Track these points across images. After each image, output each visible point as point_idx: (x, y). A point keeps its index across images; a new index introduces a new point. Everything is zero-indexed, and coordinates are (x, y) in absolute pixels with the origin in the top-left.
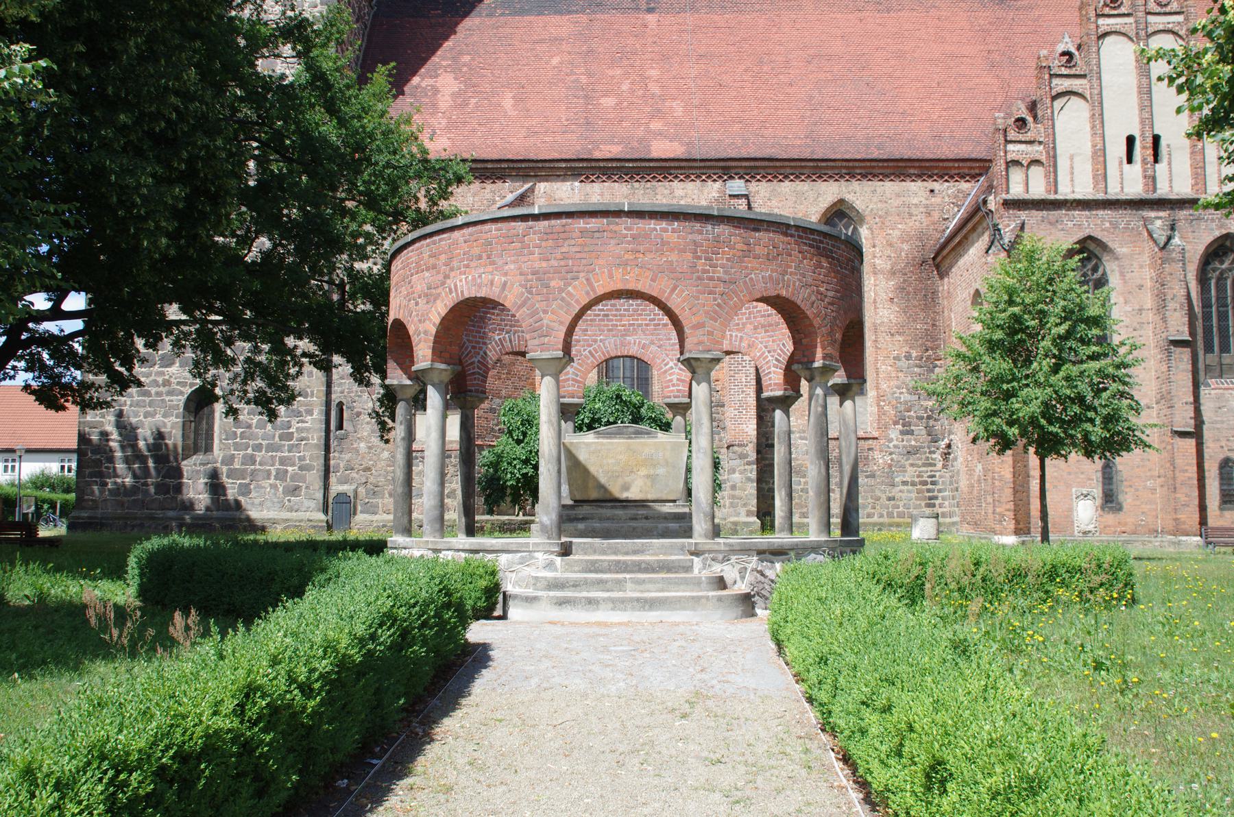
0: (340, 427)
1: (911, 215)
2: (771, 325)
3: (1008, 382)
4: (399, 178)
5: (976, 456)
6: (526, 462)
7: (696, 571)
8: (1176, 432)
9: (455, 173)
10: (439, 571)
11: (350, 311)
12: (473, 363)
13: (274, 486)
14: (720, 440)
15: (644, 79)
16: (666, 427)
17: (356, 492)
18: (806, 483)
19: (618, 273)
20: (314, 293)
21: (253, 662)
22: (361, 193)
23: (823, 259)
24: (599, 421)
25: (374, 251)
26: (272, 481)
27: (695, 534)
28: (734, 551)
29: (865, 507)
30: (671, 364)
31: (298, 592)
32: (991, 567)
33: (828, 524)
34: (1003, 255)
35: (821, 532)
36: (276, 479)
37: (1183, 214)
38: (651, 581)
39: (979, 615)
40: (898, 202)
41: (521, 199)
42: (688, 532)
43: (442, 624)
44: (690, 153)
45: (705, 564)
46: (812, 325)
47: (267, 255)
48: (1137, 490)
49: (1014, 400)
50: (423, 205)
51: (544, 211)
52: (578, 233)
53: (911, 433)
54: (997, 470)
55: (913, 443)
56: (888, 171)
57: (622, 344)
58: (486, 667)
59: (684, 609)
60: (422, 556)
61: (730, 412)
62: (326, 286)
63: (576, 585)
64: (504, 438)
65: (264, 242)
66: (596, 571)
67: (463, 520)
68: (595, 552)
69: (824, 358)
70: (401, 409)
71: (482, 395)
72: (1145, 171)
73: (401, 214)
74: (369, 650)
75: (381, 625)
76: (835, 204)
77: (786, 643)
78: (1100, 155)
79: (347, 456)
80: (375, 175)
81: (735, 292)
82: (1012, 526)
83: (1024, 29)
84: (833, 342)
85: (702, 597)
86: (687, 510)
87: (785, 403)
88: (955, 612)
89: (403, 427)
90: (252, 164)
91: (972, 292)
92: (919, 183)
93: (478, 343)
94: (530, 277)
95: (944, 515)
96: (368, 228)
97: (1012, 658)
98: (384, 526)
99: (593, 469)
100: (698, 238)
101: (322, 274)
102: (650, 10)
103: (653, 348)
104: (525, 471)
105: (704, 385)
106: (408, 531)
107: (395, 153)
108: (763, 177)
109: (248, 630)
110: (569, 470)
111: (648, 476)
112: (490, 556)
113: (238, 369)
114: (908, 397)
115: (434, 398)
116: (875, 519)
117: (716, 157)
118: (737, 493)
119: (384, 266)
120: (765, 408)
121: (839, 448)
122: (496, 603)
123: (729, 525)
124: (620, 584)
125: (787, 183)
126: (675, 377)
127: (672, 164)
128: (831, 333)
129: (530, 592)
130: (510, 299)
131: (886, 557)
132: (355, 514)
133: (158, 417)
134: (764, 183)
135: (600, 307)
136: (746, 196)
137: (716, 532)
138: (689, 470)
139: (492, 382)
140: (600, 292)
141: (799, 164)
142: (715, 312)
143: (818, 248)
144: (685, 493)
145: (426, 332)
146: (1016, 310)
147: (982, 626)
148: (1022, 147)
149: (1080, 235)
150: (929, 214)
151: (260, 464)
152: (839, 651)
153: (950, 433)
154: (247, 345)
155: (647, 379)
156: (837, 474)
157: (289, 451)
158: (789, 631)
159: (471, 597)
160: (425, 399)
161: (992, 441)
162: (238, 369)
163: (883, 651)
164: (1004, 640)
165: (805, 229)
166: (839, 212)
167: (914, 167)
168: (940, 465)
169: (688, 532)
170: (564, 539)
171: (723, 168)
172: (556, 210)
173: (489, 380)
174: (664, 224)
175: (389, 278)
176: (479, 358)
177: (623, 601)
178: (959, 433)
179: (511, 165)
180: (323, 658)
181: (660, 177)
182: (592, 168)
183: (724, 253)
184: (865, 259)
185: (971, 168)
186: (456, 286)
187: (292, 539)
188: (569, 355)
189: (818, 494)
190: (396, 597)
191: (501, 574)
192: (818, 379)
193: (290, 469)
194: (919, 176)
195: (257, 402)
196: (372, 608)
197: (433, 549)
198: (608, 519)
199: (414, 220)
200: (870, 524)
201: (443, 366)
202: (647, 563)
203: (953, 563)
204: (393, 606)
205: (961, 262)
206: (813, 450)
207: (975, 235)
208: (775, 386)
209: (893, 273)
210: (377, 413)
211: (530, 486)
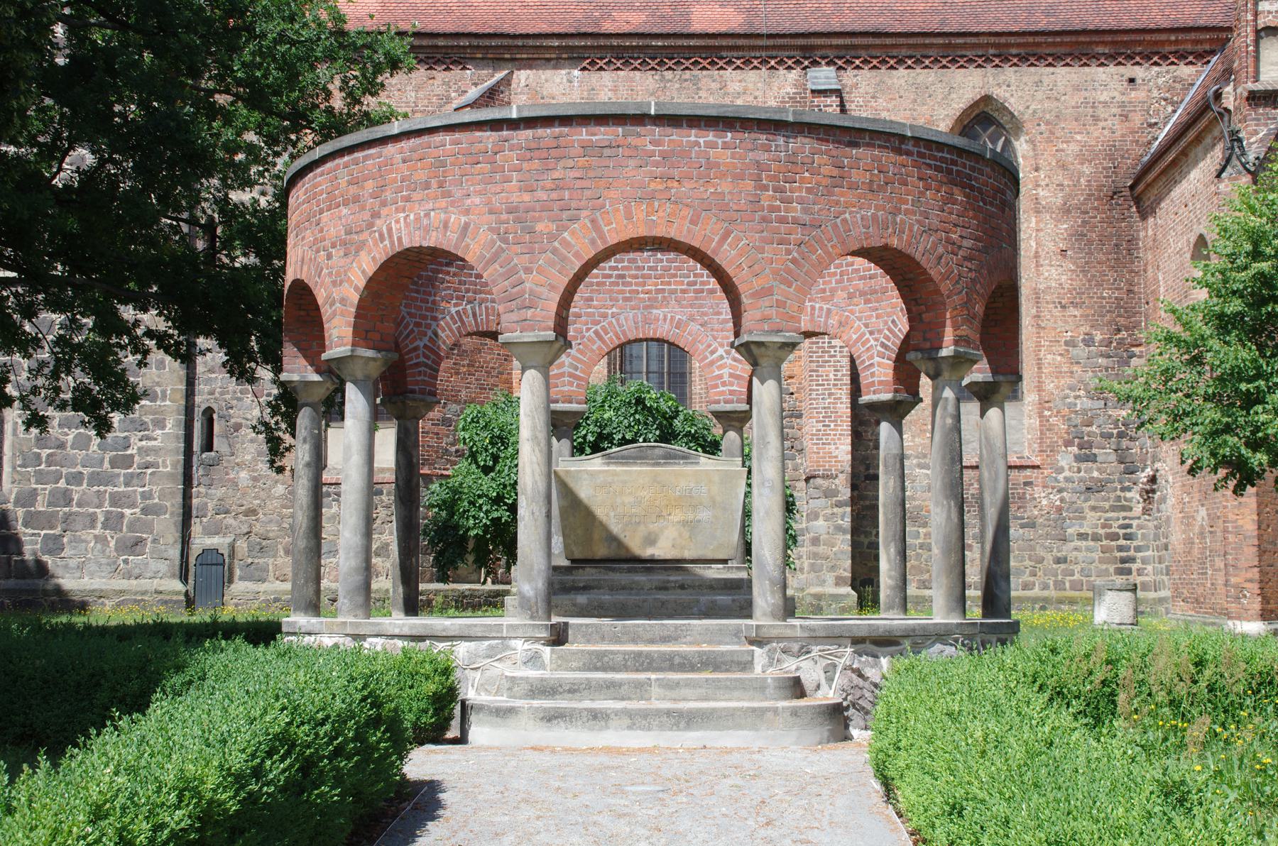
0: (208, 446)
1: (1096, 119)
2: (874, 292)
3: (1249, 381)
4: (300, 59)
5: (1197, 496)
6: (498, 500)
7: (758, 669)
9: (387, 54)
10: (362, 668)
11: (223, 266)
12: (416, 349)
13: (100, 539)
14: (795, 469)
16: (712, 448)
17: (232, 547)
18: (928, 535)
19: (640, 212)
20: (167, 238)
21: (62, 817)
22: (239, 82)
23: (956, 190)
24: (609, 438)
25: (261, 174)
26: (98, 531)
27: (757, 612)
28: (815, 639)
29: (1020, 573)
30: (721, 351)
31: (139, 704)
32: (1222, 669)
33: (963, 599)
34: (1246, 179)
35: (950, 611)
36: (105, 527)
38: (689, 684)
39: (1205, 745)
40: (1078, 98)
41: (491, 96)
42: (745, 610)
43: (366, 750)
44: (751, 24)
45: (771, 659)
46: (937, 292)
47: (88, 177)
49: (1259, 408)
50: (338, 102)
51: (526, 114)
52: (577, 150)
53: (1093, 458)
54: (1231, 517)
55: (1096, 474)
56: (1061, 50)
57: (647, 321)
58: (433, 819)
59: (739, 727)
60: (336, 646)
61: (810, 426)
62: (185, 228)
63: (573, 690)
64: (464, 464)
65: (83, 156)
66: (604, 669)
67: (401, 590)
68: (603, 639)
69: (956, 343)
70: (304, 418)
71: (430, 397)
73: (304, 117)
74: (250, 794)
75: (270, 754)
76: (976, 104)
77: (897, 783)
79: (218, 492)
80: (261, 54)
81: (819, 241)
82: (1256, 605)
84: (971, 317)
85: (767, 709)
86: (743, 575)
87: (896, 411)
88: (1165, 739)
89: (307, 447)
90: (59, 29)
91: (1193, 239)
92: (1112, 69)
93: (425, 317)
94: (504, 216)
95: (1145, 587)
96: (251, 137)
97: (1262, 815)
98: (276, 600)
99: (600, 512)
100: (763, 157)
101: (178, 209)
103: (694, 327)
104: (495, 515)
105: (771, 384)
106: (314, 607)
107: (292, 19)
108: (865, 62)
109: (55, 765)
110: (564, 513)
111: (685, 523)
112: (441, 646)
113: (45, 355)
114: (1088, 403)
115: (355, 401)
116: (1036, 592)
117: (793, 31)
118: (821, 549)
119: (277, 197)
120: (864, 420)
121: (980, 481)
122: (450, 718)
123: (809, 599)
124: (641, 689)
125: (902, 71)
126: (726, 372)
127: (724, 42)
128: (967, 304)
129: (503, 700)
130: (473, 251)
131: (1054, 651)
132: (231, 581)
134: (866, 72)
135: (612, 264)
136: (838, 93)
137: (789, 608)
138: (747, 514)
139: (445, 378)
140: (612, 240)
141: (920, 41)
142: (789, 271)
143: (949, 172)
144: (741, 549)
145: (343, 301)
146: (1265, 266)
147: (1210, 762)
150: (1125, 117)
151: (79, 505)
152: (981, 795)
153: (1155, 459)
154: (58, 318)
155: (683, 375)
156: (976, 521)
157: (127, 485)
158: (902, 764)
159: (412, 707)
160: (343, 403)
161: (1222, 472)
162: (45, 355)
163: (1051, 796)
164: (1247, 785)
165: (929, 143)
166: (984, 116)
167: (1104, 43)
168: (1138, 509)
169: (745, 610)
170: (555, 619)
171: (803, 48)
172: (545, 113)
173: (442, 375)
174: (711, 136)
175: (286, 216)
176: (426, 340)
177: (645, 714)
178: (1167, 463)
179: (475, 42)
180: (178, 807)
181: (705, 63)
182: (600, 47)
183: (803, 180)
184: (1023, 190)
185: (1197, 42)
186: (390, 230)
187: (130, 621)
188: (565, 337)
189: (947, 552)
190: (295, 709)
191: (458, 674)
192: (946, 375)
193: (127, 512)
194: (1112, 57)
195: (77, 405)
196: (257, 726)
197: (352, 635)
198: (623, 588)
199: (323, 126)
200: (1028, 599)
201: (370, 353)
202: (683, 656)
203: (1162, 661)
204: (290, 723)
205: (1176, 192)
206: (938, 485)
207: (1200, 148)
208: (880, 383)
209: (1066, 210)
210: (266, 424)
211: (501, 541)
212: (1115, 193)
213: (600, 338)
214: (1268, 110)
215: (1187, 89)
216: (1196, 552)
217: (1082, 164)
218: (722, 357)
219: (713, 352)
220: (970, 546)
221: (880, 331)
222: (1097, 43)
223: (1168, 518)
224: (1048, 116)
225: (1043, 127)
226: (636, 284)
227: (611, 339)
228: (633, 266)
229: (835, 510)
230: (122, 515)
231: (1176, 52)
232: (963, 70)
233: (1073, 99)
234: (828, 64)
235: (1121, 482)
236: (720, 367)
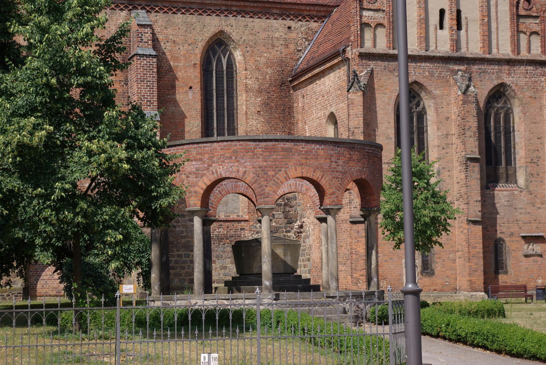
1: (273, 46)
8: (470, 221)
19: (299, 169)
37: (475, 68)
48: (444, 261)
54: (354, 247)
72: (452, 35)
78: (425, 21)
81: (346, 177)
91: (327, 114)
92: (280, 21)
94: (258, 169)
108: (161, 9)
125: (179, 15)
142: (339, 187)
145: (196, 192)
148: (371, 13)
150: (287, 46)
167: (277, 8)
185: (320, 11)
186: (217, 171)
194: (280, 15)
209: (260, 91)
212: (282, 84)
213: (220, 193)
214: (367, 61)
215: (314, 34)
217: (267, 68)
220: (215, 261)
222: (274, 8)
223: (310, 246)
224: (251, 43)
225: (249, 49)
231: (309, 15)
232: (209, 17)
233: (263, 35)
234: (142, 9)
235: (285, 228)
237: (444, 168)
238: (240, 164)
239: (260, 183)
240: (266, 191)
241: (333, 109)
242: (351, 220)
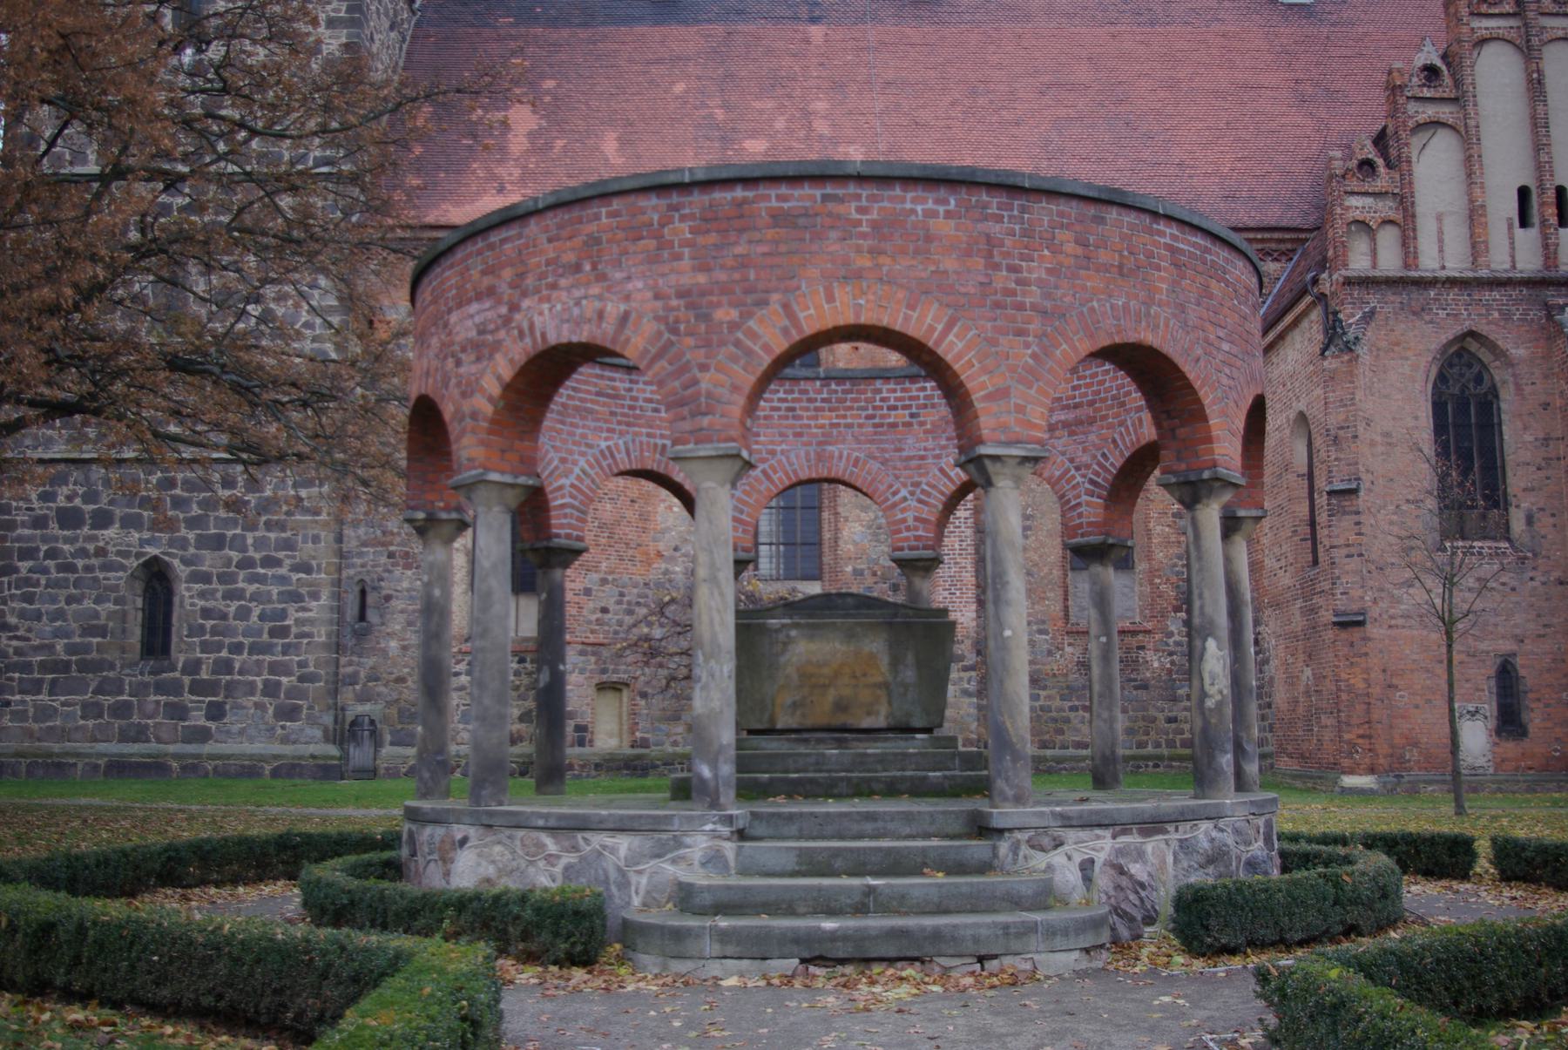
5: (1302, 657)
12: (561, 488)
13: (259, 706)
15: (807, 114)
19: (843, 294)
30: (904, 493)
54: (1344, 676)
57: (820, 457)
78: (1475, 215)
79: (370, 662)
83: (1344, 52)
91: (1292, 416)
93: (571, 452)
94: (674, 303)
102: (814, 20)
103: (875, 466)
116: (1150, 749)
126: (910, 515)
133: (88, 604)
145: (474, 415)
148: (1369, 201)
149: (1457, 330)
151: (240, 673)
157: (284, 653)
183: (1041, 257)
186: (532, 326)
193: (284, 680)
213: (769, 478)
216: (1301, 710)
218: (905, 499)
219: (895, 494)
221: (1088, 467)
226: (809, 418)
227: (780, 479)
228: (804, 397)
229: (963, 674)
230: (279, 684)
236: (903, 510)
237: (1542, 509)
238: (609, 289)
239: (682, 354)
240: (704, 386)
241: (1302, 406)
242: (634, 315)
